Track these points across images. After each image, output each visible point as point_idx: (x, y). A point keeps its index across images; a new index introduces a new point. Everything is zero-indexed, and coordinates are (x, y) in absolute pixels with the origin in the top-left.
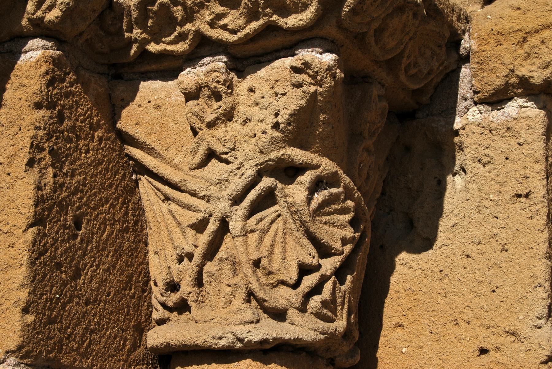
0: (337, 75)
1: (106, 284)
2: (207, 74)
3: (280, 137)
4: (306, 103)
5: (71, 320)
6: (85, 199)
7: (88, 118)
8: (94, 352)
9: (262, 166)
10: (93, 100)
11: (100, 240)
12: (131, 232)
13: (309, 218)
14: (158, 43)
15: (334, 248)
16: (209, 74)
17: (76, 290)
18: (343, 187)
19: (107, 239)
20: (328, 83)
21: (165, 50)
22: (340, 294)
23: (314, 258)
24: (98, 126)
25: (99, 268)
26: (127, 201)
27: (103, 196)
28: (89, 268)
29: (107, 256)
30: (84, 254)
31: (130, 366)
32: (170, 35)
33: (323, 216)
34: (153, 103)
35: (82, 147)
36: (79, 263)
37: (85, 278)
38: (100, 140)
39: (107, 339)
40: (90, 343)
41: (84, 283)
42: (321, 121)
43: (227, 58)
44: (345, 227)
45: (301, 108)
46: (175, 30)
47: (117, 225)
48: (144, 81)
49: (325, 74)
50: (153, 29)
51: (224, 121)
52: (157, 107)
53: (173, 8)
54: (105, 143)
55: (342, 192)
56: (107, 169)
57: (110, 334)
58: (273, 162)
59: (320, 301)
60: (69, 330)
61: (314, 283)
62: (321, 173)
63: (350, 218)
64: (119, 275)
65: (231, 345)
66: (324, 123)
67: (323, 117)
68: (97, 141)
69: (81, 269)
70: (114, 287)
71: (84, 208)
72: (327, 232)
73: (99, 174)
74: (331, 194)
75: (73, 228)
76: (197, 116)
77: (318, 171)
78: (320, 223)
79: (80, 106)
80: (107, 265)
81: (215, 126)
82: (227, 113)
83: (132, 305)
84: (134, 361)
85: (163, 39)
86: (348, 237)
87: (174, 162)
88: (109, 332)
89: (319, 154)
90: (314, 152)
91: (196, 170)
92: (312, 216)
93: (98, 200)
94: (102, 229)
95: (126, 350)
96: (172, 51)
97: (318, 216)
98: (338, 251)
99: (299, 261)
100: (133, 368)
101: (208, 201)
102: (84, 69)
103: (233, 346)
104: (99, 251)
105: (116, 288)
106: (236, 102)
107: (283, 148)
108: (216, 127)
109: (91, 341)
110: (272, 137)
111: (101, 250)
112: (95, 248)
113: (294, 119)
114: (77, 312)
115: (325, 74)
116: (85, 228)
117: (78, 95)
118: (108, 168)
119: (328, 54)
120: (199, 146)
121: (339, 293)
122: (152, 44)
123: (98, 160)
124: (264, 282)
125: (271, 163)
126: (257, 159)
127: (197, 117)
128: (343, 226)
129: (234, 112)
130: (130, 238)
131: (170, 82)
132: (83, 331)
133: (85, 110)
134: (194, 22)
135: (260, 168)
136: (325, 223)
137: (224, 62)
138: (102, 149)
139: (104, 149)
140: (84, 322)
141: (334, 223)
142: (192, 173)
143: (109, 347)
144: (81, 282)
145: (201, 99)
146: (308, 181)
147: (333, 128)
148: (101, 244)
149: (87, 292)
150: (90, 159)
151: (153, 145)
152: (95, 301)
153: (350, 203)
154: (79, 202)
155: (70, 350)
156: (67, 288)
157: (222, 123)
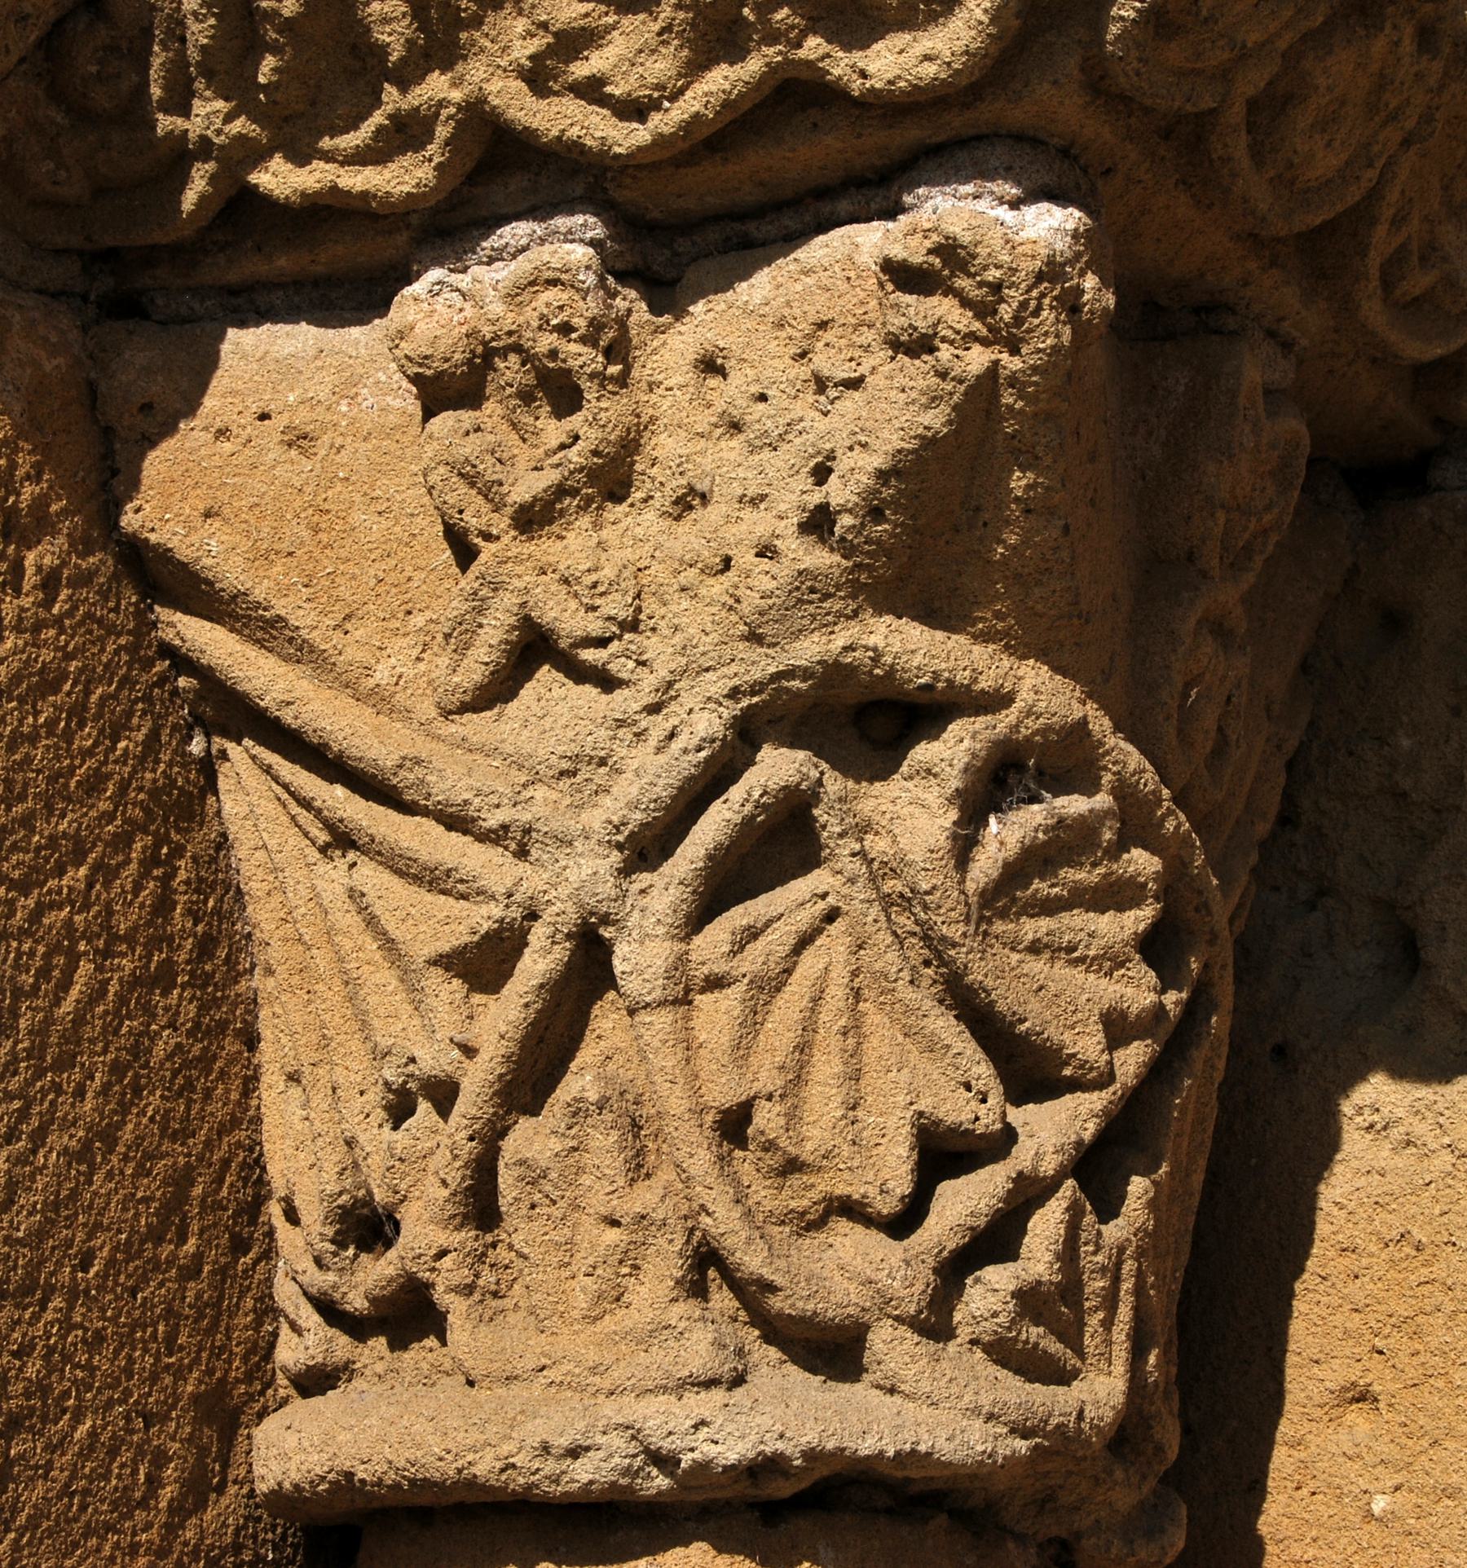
0: (1086, 297)
1: (76, 1214)
2: (516, 294)
3: (837, 573)
8: (24, 1515)
9: (755, 700)
10: (17, 408)
11: (48, 1021)
13: (962, 928)
14: (301, 157)
16: (526, 297)
19: (79, 1020)
20: (1046, 334)
21: (334, 189)
22: (1099, 1258)
23: (984, 1101)
25: (43, 1144)
26: (165, 850)
27: (61, 828)
29: (80, 1093)
32: (354, 126)
34: (278, 422)
38: (50, 583)
39: (80, 1454)
42: (1017, 499)
43: (606, 224)
44: (1122, 965)
45: (929, 442)
46: (377, 103)
47: (123, 955)
48: (242, 324)
49: (1035, 293)
50: (278, 96)
52: (299, 440)
54: (70, 598)
55: (1106, 814)
56: (78, 712)
57: (93, 1434)
58: (804, 681)
59: (1012, 1288)
61: (985, 1210)
62: (1015, 728)
64: (133, 1176)
65: (623, 1481)
66: (1028, 511)
67: (1024, 482)
68: (34, 587)
70: (109, 1229)
72: (1041, 988)
73: (43, 732)
74: (1061, 821)
76: (471, 480)
77: (1004, 721)
80: (81, 1133)
81: (551, 522)
82: (602, 466)
83: (190, 1306)
85: (326, 143)
86: (1134, 1010)
87: (371, 682)
88: (89, 1423)
89: (1007, 647)
91: (468, 716)
92: (974, 917)
93: (38, 849)
95: (163, 1504)
96: (365, 195)
97: (1003, 915)
99: (921, 1114)
101: (522, 853)
105: (119, 1231)
106: (644, 419)
107: (848, 618)
108: (555, 528)
110: (800, 573)
111: (52, 1068)
112: (28, 1058)
115: (1035, 293)
119: (1045, 206)
120: (480, 611)
121: (1095, 1253)
122: (277, 162)
124: (768, 1205)
125: (796, 684)
126: (734, 668)
127: (473, 485)
128: (1110, 962)
129: (633, 463)
131: (355, 332)
134: (459, 67)
135: (750, 706)
136: (1035, 948)
137: (592, 243)
138: (58, 622)
139: (67, 622)
141: (1071, 949)
142: (453, 728)
143: (86, 1492)
145: (490, 406)
146: (959, 765)
147: (1066, 529)
148: (53, 1040)
151: (280, 608)
153: (1142, 862)
157: (583, 508)
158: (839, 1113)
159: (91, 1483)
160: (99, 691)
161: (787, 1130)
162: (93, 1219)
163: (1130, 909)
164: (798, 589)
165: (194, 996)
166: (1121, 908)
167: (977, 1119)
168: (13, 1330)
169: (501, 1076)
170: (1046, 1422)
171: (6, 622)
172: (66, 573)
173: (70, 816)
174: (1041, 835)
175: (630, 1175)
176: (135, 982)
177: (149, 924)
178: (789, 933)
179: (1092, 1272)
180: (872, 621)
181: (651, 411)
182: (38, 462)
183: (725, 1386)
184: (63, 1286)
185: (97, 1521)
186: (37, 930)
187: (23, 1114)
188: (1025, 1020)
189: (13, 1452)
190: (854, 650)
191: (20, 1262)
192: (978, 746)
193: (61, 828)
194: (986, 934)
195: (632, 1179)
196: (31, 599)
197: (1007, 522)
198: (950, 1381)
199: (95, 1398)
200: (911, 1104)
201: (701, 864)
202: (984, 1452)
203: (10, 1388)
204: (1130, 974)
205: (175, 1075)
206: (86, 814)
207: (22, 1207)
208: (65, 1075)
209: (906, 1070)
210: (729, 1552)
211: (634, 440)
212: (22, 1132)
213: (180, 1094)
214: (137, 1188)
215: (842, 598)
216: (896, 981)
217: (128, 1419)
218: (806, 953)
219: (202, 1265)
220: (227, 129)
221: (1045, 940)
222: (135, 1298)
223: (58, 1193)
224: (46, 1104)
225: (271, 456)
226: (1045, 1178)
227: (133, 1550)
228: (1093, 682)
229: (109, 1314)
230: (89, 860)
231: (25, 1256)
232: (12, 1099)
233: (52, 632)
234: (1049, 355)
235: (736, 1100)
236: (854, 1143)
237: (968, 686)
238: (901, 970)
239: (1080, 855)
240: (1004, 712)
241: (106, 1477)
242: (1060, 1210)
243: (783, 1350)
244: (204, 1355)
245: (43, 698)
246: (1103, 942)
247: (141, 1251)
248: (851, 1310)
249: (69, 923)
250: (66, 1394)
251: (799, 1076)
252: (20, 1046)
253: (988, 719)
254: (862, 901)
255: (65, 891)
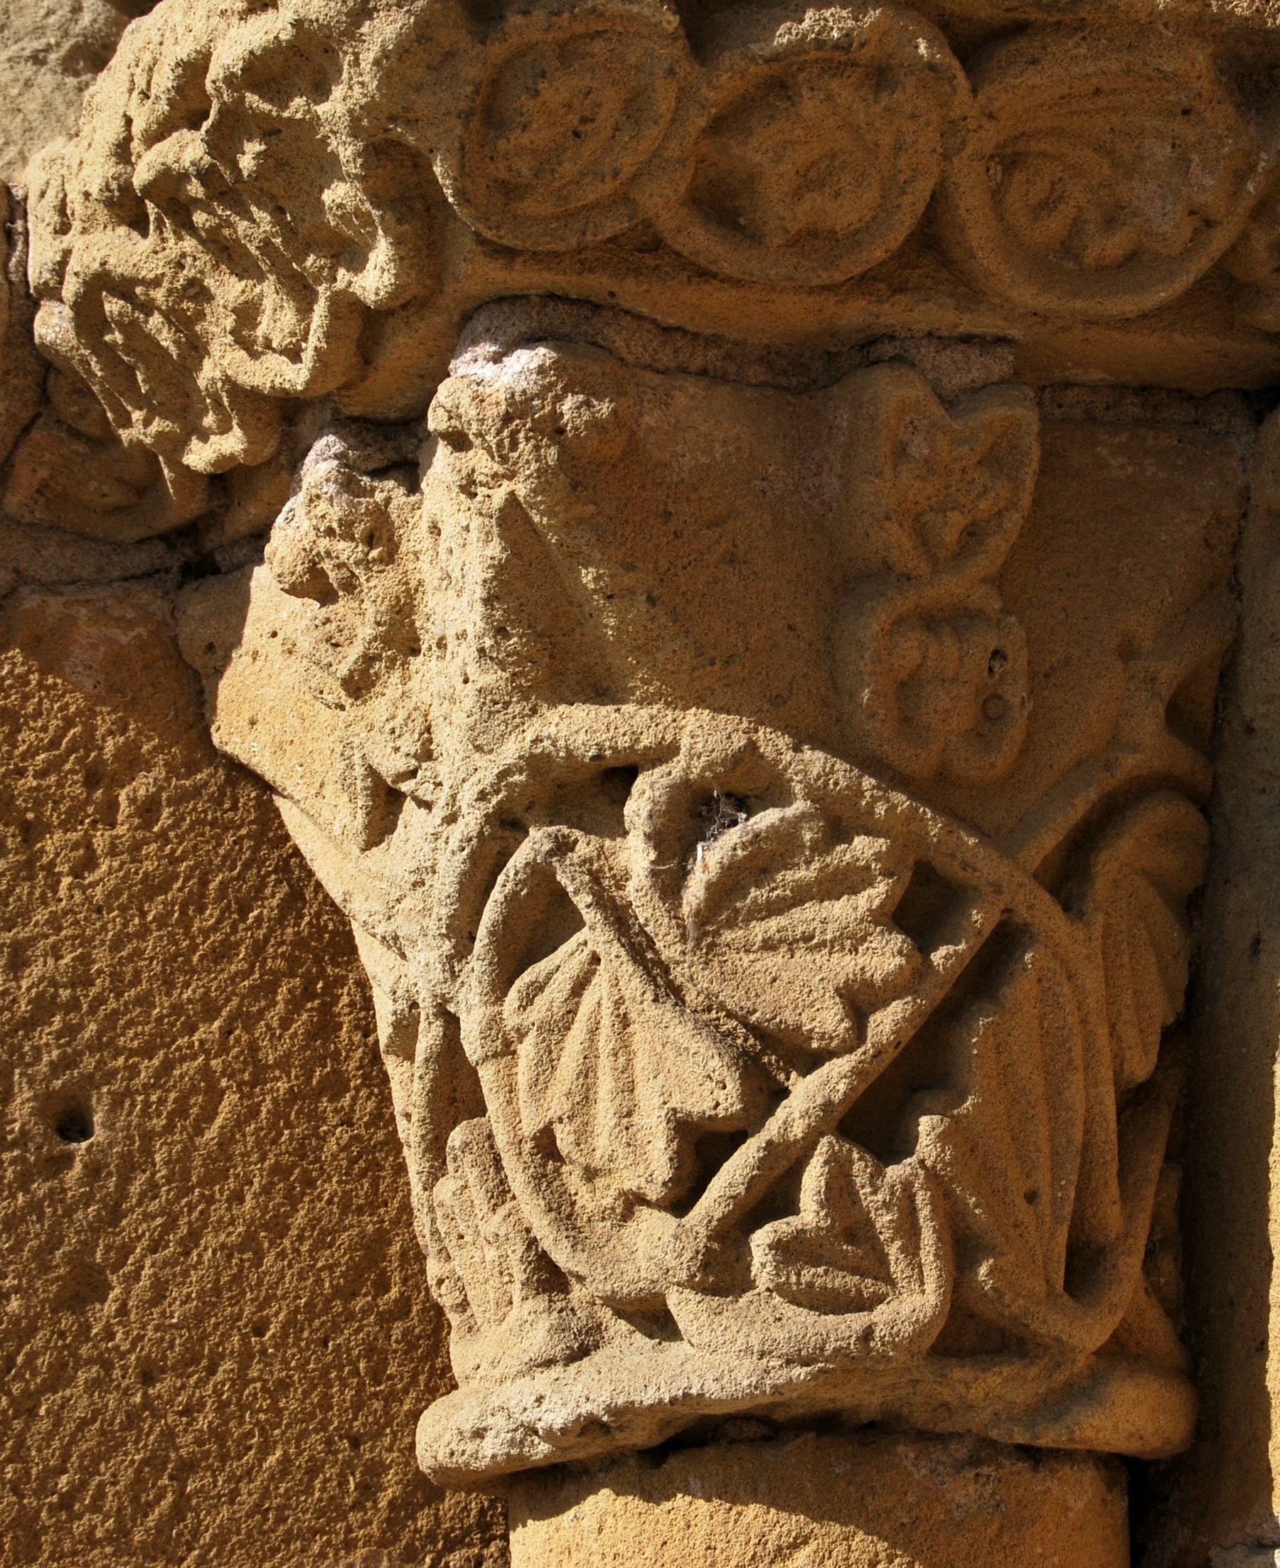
0: (566, 417)
1: (243, 1293)
3: (502, 683)
4: (504, 549)
5: (70, 1444)
6: (93, 1027)
7: (71, 750)
8: (208, 1535)
9: (500, 796)
10: (88, 684)
11: (189, 1149)
12: (357, 1089)
13: (679, 947)
15: (811, 1030)
17: (87, 1341)
18: (807, 796)
19: (225, 1141)
20: (528, 462)
22: (880, 1197)
23: (724, 1087)
24: (131, 762)
25: (197, 1246)
26: (320, 985)
27: (185, 996)
28: (143, 1256)
29: (238, 1197)
30: (114, 1214)
31: (411, 1554)
33: (753, 923)
35: (57, 855)
36: (87, 1247)
37: (127, 1291)
38: (147, 810)
39: (272, 1478)
40: (178, 1512)
41: (123, 1311)
42: (595, 591)
44: (863, 939)
45: (500, 569)
47: (278, 1079)
49: (505, 433)
51: (392, 661)
53: (146, 322)
54: (172, 814)
55: (802, 817)
56: (197, 901)
57: (286, 1460)
58: (521, 774)
59: (768, 1241)
60: (64, 1479)
61: (740, 1180)
62: (687, 769)
63: (876, 902)
64: (310, 1251)
65: (514, 1451)
66: (610, 597)
67: (590, 577)
68: (129, 816)
69: (101, 1270)
70: (284, 1297)
71: (89, 1063)
72: (774, 980)
73: (153, 926)
74: (757, 835)
75: (39, 1140)
77: (677, 767)
78: (747, 951)
79: (26, 723)
80: (240, 1229)
81: (373, 685)
82: (388, 632)
83: (397, 1342)
84: (431, 1537)
86: (878, 977)
88: (278, 1453)
89: (668, 704)
90: (644, 701)
92: (692, 933)
93: (160, 1019)
94: (195, 1110)
95: (383, 1504)
97: (731, 924)
98: (831, 1038)
99: (674, 1110)
100: (428, 1560)
102: (51, 588)
103: (521, 1457)
104: (193, 1187)
105: (298, 1297)
106: (413, 584)
107: (530, 716)
108: (378, 689)
109: (182, 1497)
110: (480, 691)
111: (199, 1184)
113: (505, 611)
114: (96, 1413)
115: (505, 433)
116: (103, 1124)
117: (11, 687)
118: (203, 895)
121: (874, 1193)
123: (142, 881)
124: (590, 1207)
126: (478, 775)
128: (853, 940)
129: (413, 622)
130: (352, 1110)
132: (139, 1471)
133: (51, 729)
135: (498, 803)
136: (769, 945)
137: (336, 457)
138: (163, 836)
139: (172, 834)
140: (136, 1442)
141: (807, 938)
143: (280, 1508)
144: (110, 1307)
146: (644, 814)
147: (651, 600)
149: (140, 1338)
150: (99, 889)
152: (191, 1358)
153: (863, 847)
154: (59, 1047)
155: (80, 1542)
156: (39, 1340)
158: (612, 1123)
159: (289, 1499)
160: (218, 879)
161: (578, 1145)
162: (264, 1293)
163: (864, 889)
164: (484, 703)
165: (372, 1093)
166: (854, 891)
167: (718, 1104)
168: (179, 1395)
169: (423, 1136)
170: (822, 1349)
171: (99, 852)
172: (164, 795)
173: (194, 985)
174: (739, 852)
175: (493, 1201)
176: (292, 1096)
177: (303, 1049)
178: (565, 980)
179: (877, 1209)
180: (548, 714)
181: (418, 576)
182: (121, 718)
183: (561, 1363)
184: (232, 1352)
185: (300, 1528)
186: (166, 1082)
187: (171, 1225)
188: (755, 1011)
189: (189, 1489)
190: (542, 741)
191: (177, 1342)
192: (657, 794)
193: (185, 996)
194: (711, 946)
195: (495, 1205)
196: (126, 826)
197: (601, 611)
198: (726, 1329)
199: (283, 1433)
200: (665, 1103)
201: (487, 941)
202: (750, 1385)
203: (178, 1441)
204: (873, 945)
205: (352, 1162)
206: (216, 978)
207: (175, 1299)
208: (217, 1187)
209: (661, 1075)
210: (623, 1495)
211: (405, 604)
212: (169, 1241)
213: (363, 1174)
214: (317, 1260)
215: (518, 702)
216: (642, 1002)
217: (329, 1442)
218: (586, 992)
219: (410, 1306)
220: (148, 430)
221: (777, 936)
222: (327, 1347)
223: (218, 1280)
224: (195, 1214)
225: (278, 665)
226: (796, 1141)
227: (350, 1545)
228: (760, 710)
229: (293, 1364)
230: (224, 1014)
231: (181, 1336)
232: (154, 1218)
233: (153, 847)
234: (538, 477)
235: (536, 1129)
236: (629, 1145)
237: (631, 747)
238: (644, 993)
239: (791, 858)
240: (675, 760)
241: (309, 1491)
242: (820, 1164)
243: (630, 1321)
244: (422, 1378)
245: (151, 899)
246: (836, 925)
247: (326, 1310)
248: (641, 1285)
249: (205, 1070)
250: (250, 1434)
251: (587, 1098)
252: (159, 1175)
253: (663, 769)
254: (604, 943)
255: (197, 1044)
